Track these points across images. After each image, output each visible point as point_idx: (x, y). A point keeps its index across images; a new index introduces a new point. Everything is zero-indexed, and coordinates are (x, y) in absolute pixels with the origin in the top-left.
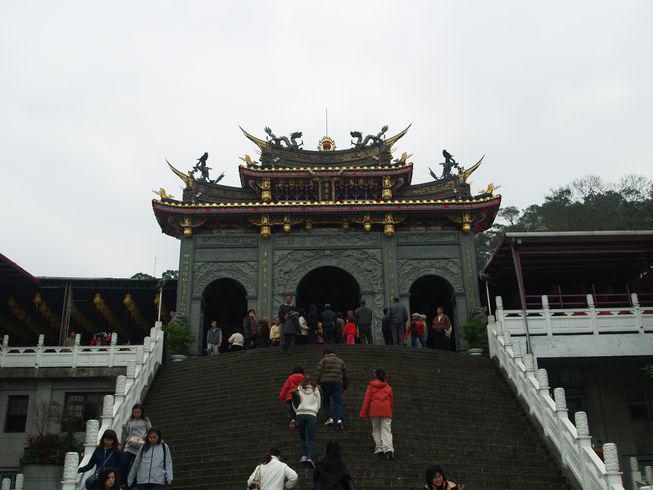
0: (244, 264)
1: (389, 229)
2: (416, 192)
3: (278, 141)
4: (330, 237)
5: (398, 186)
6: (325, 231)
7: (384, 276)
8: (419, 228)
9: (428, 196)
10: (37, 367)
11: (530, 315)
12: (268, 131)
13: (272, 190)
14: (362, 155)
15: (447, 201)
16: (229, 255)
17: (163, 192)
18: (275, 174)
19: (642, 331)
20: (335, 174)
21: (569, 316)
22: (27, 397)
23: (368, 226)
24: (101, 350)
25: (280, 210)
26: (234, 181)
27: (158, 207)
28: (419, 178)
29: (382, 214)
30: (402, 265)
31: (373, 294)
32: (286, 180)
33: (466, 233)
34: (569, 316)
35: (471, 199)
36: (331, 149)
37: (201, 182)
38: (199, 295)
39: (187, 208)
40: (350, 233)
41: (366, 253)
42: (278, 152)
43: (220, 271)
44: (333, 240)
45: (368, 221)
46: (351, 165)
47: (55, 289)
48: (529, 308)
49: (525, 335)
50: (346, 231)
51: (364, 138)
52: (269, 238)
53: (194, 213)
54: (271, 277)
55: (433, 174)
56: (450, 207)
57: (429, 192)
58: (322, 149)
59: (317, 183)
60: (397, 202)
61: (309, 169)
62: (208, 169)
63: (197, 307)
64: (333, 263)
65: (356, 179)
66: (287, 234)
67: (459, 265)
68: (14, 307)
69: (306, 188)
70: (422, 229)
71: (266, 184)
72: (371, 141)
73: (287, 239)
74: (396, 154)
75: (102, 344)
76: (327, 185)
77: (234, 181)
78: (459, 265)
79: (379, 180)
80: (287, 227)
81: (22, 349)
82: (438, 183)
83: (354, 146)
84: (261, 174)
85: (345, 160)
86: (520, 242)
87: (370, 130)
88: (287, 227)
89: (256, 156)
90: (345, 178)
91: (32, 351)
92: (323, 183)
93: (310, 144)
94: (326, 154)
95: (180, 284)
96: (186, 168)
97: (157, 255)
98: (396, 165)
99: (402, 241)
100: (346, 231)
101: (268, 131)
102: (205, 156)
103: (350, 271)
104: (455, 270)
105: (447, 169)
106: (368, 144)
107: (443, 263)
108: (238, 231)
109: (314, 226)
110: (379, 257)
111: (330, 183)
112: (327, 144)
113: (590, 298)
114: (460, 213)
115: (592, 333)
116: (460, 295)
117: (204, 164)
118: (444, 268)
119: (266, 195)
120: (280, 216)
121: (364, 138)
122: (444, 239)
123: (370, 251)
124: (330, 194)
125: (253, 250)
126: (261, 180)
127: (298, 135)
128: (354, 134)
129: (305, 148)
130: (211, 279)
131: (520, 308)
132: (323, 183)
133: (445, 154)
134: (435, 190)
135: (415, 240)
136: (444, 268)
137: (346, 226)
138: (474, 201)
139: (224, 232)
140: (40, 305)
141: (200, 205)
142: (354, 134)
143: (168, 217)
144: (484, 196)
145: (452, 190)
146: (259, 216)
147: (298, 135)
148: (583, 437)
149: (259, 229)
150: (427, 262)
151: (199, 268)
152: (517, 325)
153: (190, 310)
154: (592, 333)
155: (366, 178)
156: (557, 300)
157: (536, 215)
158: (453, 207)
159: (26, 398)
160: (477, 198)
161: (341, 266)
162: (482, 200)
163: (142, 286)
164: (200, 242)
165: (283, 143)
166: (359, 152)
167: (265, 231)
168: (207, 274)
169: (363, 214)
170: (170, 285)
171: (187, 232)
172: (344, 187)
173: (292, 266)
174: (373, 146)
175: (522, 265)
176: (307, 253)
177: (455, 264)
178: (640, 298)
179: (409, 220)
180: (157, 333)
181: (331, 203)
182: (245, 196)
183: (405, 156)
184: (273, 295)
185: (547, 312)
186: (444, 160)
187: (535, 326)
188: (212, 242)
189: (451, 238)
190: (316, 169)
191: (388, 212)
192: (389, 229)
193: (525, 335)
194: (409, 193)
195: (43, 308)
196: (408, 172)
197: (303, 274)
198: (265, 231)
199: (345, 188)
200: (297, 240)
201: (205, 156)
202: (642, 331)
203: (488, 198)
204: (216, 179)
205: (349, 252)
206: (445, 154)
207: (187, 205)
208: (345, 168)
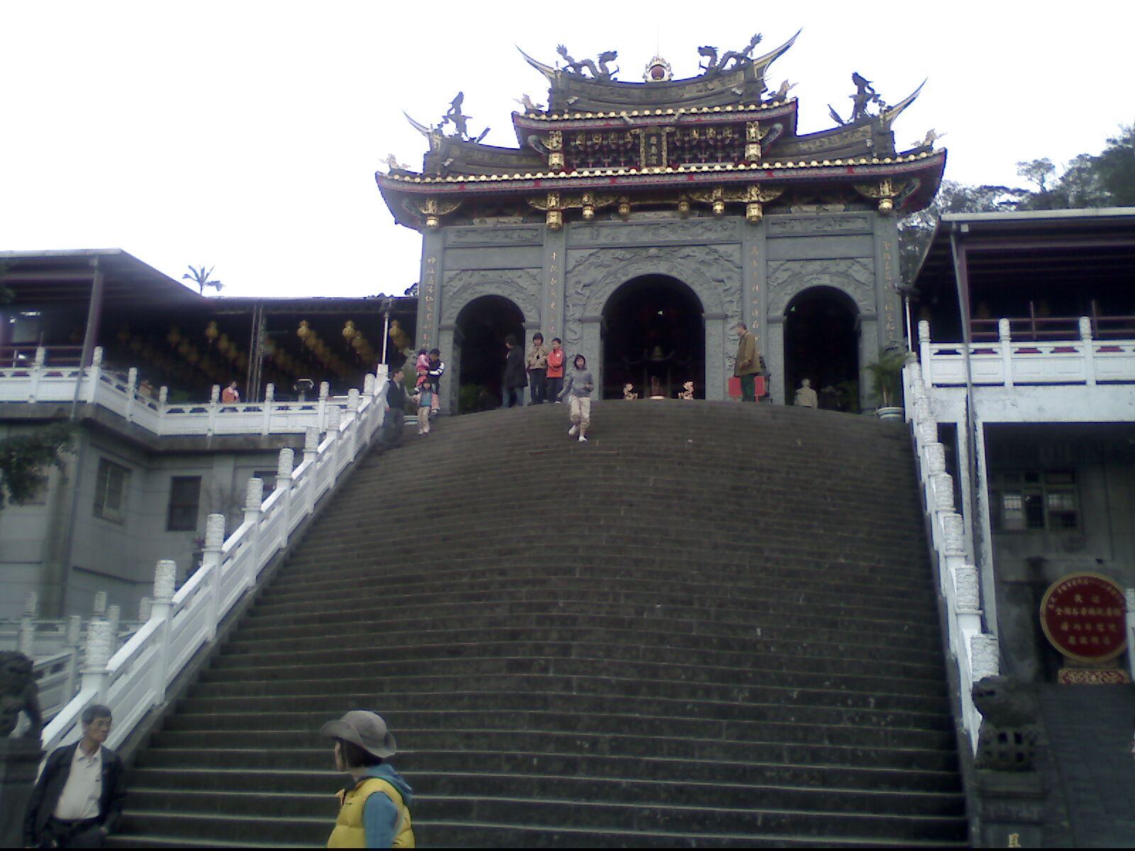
0: (520, 272)
1: (754, 211)
2: (804, 147)
3: (578, 67)
4: (655, 225)
5: (773, 138)
6: (651, 216)
7: (743, 291)
8: (805, 208)
9: (820, 154)
10: (210, 434)
11: (976, 352)
12: (562, 51)
13: (566, 151)
14: (715, 85)
15: (851, 162)
16: (498, 258)
17: (392, 159)
18: (568, 124)
19: (1009, 383)
20: (667, 120)
21: (1046, 353)
22: (197, 480)
23: (719, 208)
24: (304, 408)
25: (574, 183)
26: (507, 138)
27: (385, 183)
28: (811, 121)
29: (742, 187)
30: (776, 270)
31: (725, 317)
32: (589, 133)
33: (885, 214)
34: (1046, 353)
35: (894, 156)
36: (666, 78)
37: (455, 141)
38: (452, 322)
39: (430, 183)
40: (692, 219)
41: (716, 251)
42: (578, 86)
43: (482, 284)
44: (663, 231)
45: (717, 200)
46: (693, 105)
47: (237, 319)
48: (975, 340)
49: (964, 385)
50: (685, 216)
51: (720, 55)
52: (558, 230)
53: (453, 192)
54: (562, 293)
55: (836, 117)
56: (858, 171)
57: (827, 145)
58: (650, 79)
59: (637, 137)
60: (766, 166)
61: (623, 114)
62: (465, 118)
63: (447, 346)
64: (662, 268)
65: (702, 127)
66: (718, 217)
67: (867, 264)
68: (179, 344)
69: (621, 146)
70: (811, 210)
71: (555, 142)
72: (732, 61)
73: (587, 230)
74: (773, 81)
75: (307, 400)
76: (654, 140)
77: (507, 138)
78: (867, 264)
79: (741, 128)
80: (588, 212)
81: (188, 408)
82: (844, 129)
83: (702, 71)
84: (547, 126)
85: (687, 96)
86: (965, 229)
87: (730, 42)
88: (588, 212)
89: (541, 99)
90: (685, 128)
91: (202, 410)
92: (648, 137)
93: (631, 70)
94: (658, 89)
95: (421, 306)
96: (432, 118)
97: (382, 261)
98: (769, 102)
99: (777, 230)
100: (685, 216)
101: (562, 51)
102: (460, 98)
103: (688, 282)
104: (862, 276)
105: (860, 105)
106: (728, 67)
107: (843, 266)
108: (512, 219)
109: (633, 209)
110: (736, 257)
111: (659, 136)
112: (657, 69)
113: (1085, 324)
114: (876, 181)
115: (1083, 383)
116: (715, 317)
117: (458, 111)
118: (845, 274)
119: (555, 160)
120: (577, 193)
121: (720, 55)
122: (846, 226)
123: (721, 249)
124: (659, 155)
125: (537, 248)
126: (546, 134)
127: (611, 56)
128: (703, 51)
129: (621, 77)
130: (469, 297)
131: (960, 340)
132: (648, 137)
133: (857, 79)
134: (837, 141)
135: (798, 228)
136: (845, 274)
137: (684, 208)
138: (899, 160)
139: (491, 222)
140: (217, 340)
141: (449, 179)
142: (703, 51)
143: (404, 197)
144: (915, 152)
145: (865, 142)
146: (542, 195)
147: (611, 56)
148: (953, 553)
149: (543, 215)
150: (816, 266)
151: (451, 279)
152: (952, 369)
153: (438, 343)
154: (1083, 383)
155: (719, 127)
156: (1026, 326)
157: (1090, 172)
158: (868, 172)
159: (197, 480)
160: (905, 154)
161: (674, 274)
162: (912, 157)
163: (367, 313)
164: (452, 238)
165: (586, 71)
166: (710, 80)
167: (553, 218)
168: (464, 288)
169: (708, 188)
170: (405, 309)
171: (431, 222)
172: (684, 142)
173: (597, 274)
174: (735, 69)
175: (970, 267)
176: (619, 253)
177: (864, 266)
178: (1013, 327)
179: (790, 193)
180: (377, 383)
181: (657, 170)
182: (524, 162)
183: (785, 86)
184: (565, 321)
185: (1005, 347)
186: (854, 90)
187: (984, 368)
188: (471, 238)
189: (859, 225)
190: (635, 113)
191: (753, 183)
192: (754, 211)
193: (964, 385)
194: (793, 149)
195: (224, 344)
196: (790, 117)
197: (613, 287)
198: (553, 218)
199: (683, 145)
200: (605, 231)
201: (460, 98)
202: (1091, 382)
203: (924, 155)
204: (477, 135)
205: (687, 251)
206: (857, 79)
207: (428, 180)
208: (683, 111)
